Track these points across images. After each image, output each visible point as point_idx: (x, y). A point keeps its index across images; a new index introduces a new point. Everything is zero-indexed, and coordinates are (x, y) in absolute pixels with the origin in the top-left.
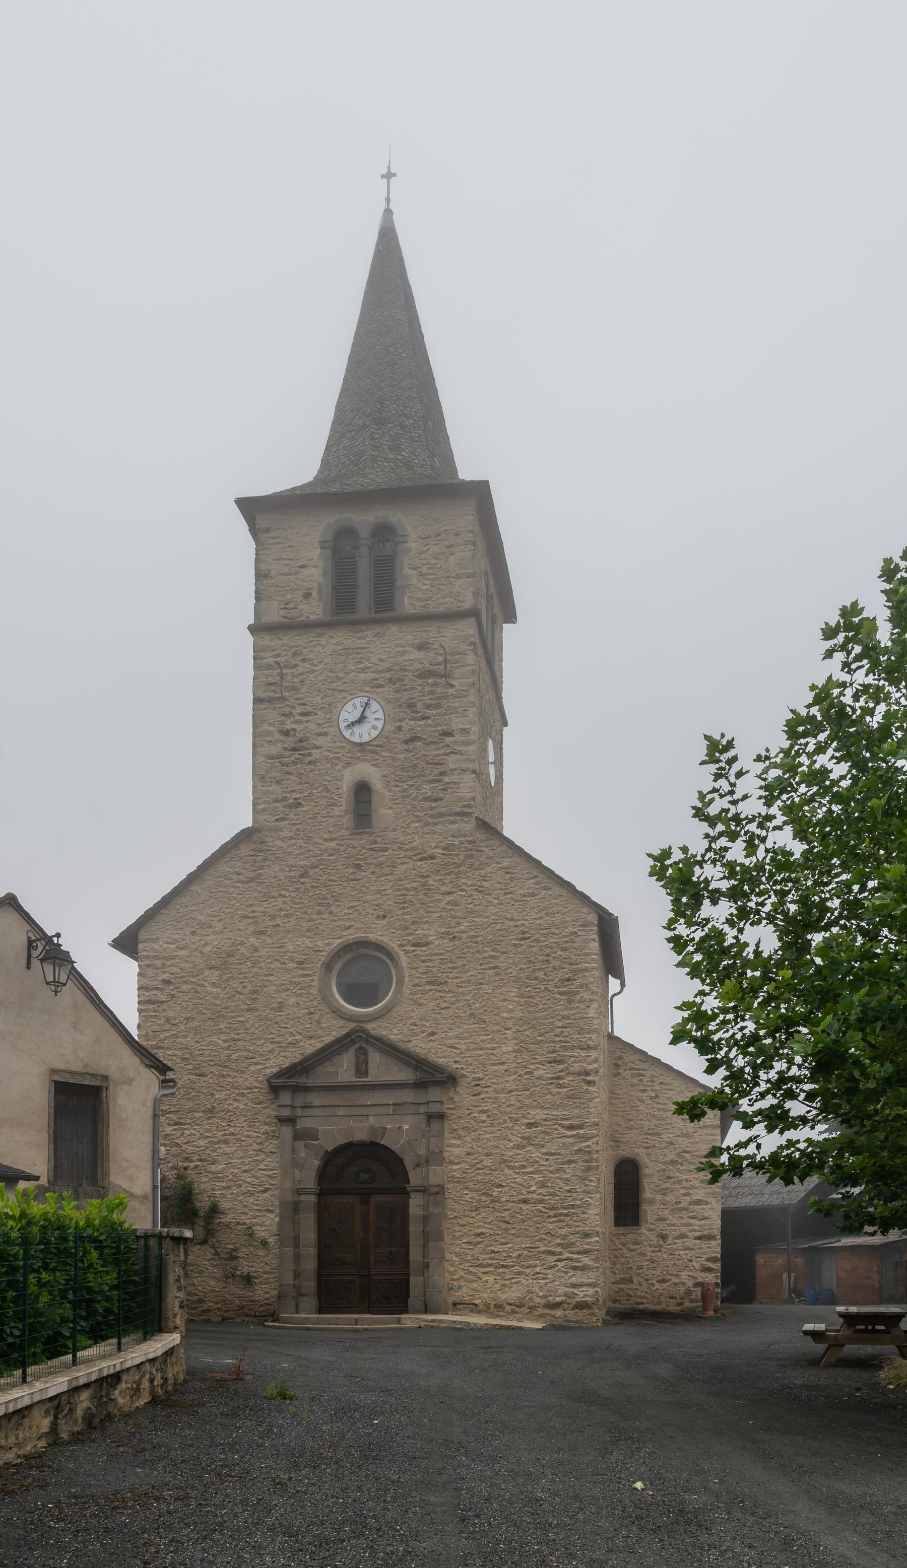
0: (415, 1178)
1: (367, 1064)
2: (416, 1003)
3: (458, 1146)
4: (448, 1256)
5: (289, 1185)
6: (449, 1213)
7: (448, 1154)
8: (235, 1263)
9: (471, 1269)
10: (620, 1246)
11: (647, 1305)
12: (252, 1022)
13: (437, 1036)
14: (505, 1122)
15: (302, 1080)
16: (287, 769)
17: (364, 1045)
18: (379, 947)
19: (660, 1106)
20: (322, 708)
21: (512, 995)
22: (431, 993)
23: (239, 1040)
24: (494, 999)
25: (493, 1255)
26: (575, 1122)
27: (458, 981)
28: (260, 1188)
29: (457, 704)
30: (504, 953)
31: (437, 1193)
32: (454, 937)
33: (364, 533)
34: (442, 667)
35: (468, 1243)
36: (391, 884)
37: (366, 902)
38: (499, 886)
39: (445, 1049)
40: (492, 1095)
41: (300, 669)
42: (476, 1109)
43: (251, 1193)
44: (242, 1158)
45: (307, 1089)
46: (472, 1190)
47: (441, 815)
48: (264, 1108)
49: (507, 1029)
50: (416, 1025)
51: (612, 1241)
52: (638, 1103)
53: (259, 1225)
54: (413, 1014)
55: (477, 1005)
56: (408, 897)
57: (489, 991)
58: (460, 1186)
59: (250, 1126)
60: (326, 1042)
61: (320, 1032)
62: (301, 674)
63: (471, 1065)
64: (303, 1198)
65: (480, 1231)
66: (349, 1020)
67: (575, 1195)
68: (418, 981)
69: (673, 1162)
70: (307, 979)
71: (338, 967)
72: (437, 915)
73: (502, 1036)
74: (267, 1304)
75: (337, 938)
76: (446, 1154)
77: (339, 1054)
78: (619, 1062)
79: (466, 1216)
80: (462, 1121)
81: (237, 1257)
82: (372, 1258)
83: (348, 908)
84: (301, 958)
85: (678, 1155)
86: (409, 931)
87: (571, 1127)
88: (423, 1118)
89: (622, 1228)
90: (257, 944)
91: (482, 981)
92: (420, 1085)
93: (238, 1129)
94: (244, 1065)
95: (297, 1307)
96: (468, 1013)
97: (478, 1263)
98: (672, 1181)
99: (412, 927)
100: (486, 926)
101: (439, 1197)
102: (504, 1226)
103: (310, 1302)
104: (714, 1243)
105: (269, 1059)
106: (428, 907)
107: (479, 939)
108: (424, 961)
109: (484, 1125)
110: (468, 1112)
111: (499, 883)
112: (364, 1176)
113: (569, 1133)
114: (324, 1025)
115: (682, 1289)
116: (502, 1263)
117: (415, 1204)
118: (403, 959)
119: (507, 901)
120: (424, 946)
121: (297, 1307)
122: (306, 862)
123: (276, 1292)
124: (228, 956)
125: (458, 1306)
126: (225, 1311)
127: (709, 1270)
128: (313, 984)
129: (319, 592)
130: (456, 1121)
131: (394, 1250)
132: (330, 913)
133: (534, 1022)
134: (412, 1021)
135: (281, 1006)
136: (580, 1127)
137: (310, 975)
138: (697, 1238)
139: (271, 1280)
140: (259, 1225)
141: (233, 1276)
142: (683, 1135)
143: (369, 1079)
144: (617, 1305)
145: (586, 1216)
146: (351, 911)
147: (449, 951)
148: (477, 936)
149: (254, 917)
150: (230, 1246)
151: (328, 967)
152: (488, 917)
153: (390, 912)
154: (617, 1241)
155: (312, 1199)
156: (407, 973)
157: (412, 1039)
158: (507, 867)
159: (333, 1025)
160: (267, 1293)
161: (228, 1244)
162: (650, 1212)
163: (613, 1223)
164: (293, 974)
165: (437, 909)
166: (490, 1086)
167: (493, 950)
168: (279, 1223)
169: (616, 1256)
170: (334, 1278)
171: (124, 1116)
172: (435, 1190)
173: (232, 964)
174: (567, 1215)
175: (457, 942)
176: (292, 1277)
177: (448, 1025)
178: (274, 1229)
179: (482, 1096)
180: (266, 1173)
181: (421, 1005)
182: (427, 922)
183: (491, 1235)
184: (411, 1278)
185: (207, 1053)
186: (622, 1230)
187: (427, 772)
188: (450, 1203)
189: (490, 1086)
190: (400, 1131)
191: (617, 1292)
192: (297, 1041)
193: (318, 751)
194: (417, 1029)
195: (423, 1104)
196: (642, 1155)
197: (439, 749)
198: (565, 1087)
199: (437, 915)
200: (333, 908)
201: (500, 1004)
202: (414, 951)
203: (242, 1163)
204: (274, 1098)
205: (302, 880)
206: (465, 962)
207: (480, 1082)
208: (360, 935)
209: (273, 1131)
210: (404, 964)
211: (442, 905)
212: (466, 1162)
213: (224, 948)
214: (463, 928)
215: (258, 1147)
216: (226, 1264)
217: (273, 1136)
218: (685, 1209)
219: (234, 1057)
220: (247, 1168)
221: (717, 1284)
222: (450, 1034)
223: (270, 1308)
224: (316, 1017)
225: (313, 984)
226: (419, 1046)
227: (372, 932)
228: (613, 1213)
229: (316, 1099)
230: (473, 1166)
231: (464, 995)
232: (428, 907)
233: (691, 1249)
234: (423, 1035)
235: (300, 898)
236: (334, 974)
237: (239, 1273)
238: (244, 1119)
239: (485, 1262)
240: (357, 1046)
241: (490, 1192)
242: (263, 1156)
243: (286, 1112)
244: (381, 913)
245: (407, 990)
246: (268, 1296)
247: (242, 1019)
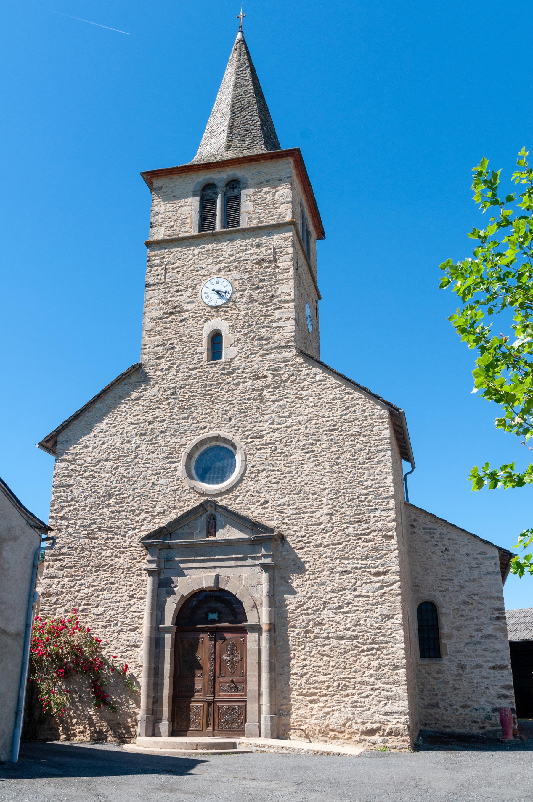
10: (427, 675)
11: (453, 729)
16: (166, 325)
18: (226, 440)
19: (450, 557)
20: (191, 287)
21: (326, 471)
23: (122, 511)
26: (381, 569)
29: (281, 278)
33: (221, 185)
34: (272, 256)
36: (235, 396)
39: (275, 513)
41: (177, 265)
47: (272, 349)
50: (252, 496)
51: (419, 670)
52: (432, 555)
60: (185, 511)
62: (178, 267)
67: (383, 631)
69: (465, 603)
78: (415, 524)
85: (469, 596)
87: (377, 574)
89: (427, 659)
91: (303, 462)
95: (154, 730)
98: (465, 618)
104: (505, 672)
108: (259, 449)
111: (314, 391)
113: (376, 579)
115: (483, 714)
122: (176, 385)
127: (505, 697)
129: (191, 219)
133: (345, 491)
134: (249, 492)
136: (385, 573)
138: (491, 668)
142: (470, 580)
144: (427, 728)
145: (394, 650)
147: (277, 441)
154: (423, 671)
158: (320, 381)
162: (448, 644)
163: (418, 655)
169: (423, 684)
171: (7, 566)
174: (378, 649)
182: (261, 422)
185: (98, 521)
186: (426, 661)
187: (262, 321)
191: (427, 716)
193: (187, 313)
196: (439, 598)
197: (269, 306)
198: (370, 541)
202: (251, 442)
205: (173, 397)
208: (213, 433)
211: (272, 409)
218: (479, 643)
219: (118, 524)
221: (512, 709)
226: (254, 513)
228: (418, 647)
230: (299, 607)
233: (487, 678)
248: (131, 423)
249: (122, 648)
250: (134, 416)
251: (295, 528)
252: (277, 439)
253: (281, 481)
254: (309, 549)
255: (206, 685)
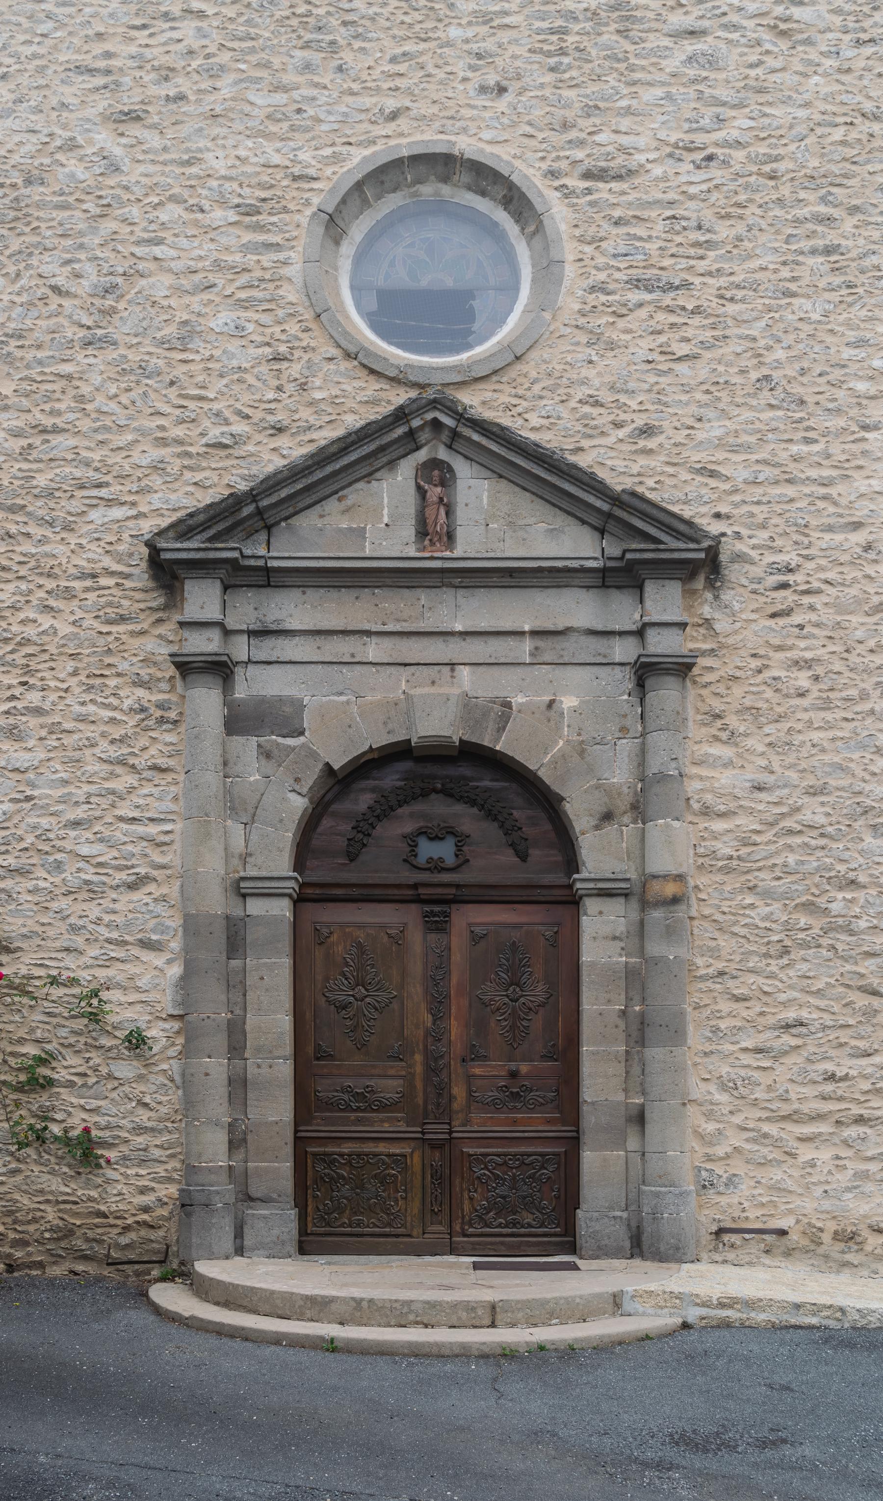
0: (600, 854)
1: (449, 512)
2: (595, 338)
3: (728, 764)
4: (698, 1090)
5: (214, 866)
6: (700, 961)
7: (697, 785)
8: (43, 1099)
9: (766, 1128)
12: (97, 380)
13: (661, 439)
14: (864, 696)
15: (256, 549)
17: (443, 454)
22: (643, 313)
23: (56, 430)
24: (829, 339)
25: (829, 1088)
27: (723, 281)
28: (123, 876)
30: (854, 210)
31: (675, 900)
32: (710, 158)
35: (759, 1051)
37: (449, 44)
38: (838, 20)
39: (685, 476)
40: (828, 616)
42: (780, 655)
43: (92, 891)
44: (65, 782)
45: (268, 578)
46: (768, 895)
48: (133, 634)
49: (865, 428)
50: (597, 404)
53: (119, 986)
54: (590, 372)
55: (780, 354)
56: (571, 39)
57: (815, 316)
58: (732, 882)
59: (90, 688)
61: (306, 414)
63: (763, 526)
64: (255, 907)
65: (791, 1015)
66: (395, 381)
68: (602, 276)
70: (267, 259)
71: (358, 231)
72: (659, 92)
73: (856, 448)
74: (145, 1224)
75: (359, 144)
76: (692, 787)
77: (368, 477)
79: (751, 971)
80: (738, 691)
81: (50, 1083)
82: (459, 1091)
83: (393, 60)
84: (251, 196)
86: (573, 134)
88: (625, 680)
90: (118, 151)
91: (793, 287)
92: (621, 577)
93: (53, 697)
94: (75, 506)
95: (239, 1234)
96: (754, 375)
97: (786, 1109)
99: (586, 124)
100: (801, 129)
101: (680, 912)
102: (862, 1001)
103: (280, 1220)
105: (149, 490)
106: (632, 69)
107: (782, 166)
109: (805, 702)
110: (755, 663)
112: (445, 850)
114: (318, 395)
116: (856, 1110)
117: (601, 934)
118: (559, 214)
119: (862, 64)
120: (619, 177)
121: (239, 1234)
123: (173, 1190)
124: (28, 182)
125: (726, 1238)
126: (16, 1243)
128: (286, 271)
130: (721, 690)
131: (524, 1068)
132: (340, 69)
135: (189, 332)
137: (276, 247)
139: (157, 1153)
140: (119, 986)
141: (40, 1138)
143: (458, 552)
146: (402, 68)
147: (692, 198)
148: (777, 159)
149: (108, 72)
150: (32, 1050)
151: (333, 225)
152: (807, 105)
153: (519, 77)
155: (282, 909)
156: (569, 251)
157: (585, 443)
159: (344, 394)
160: (143, 1191)
161: (21, 1041)
164: (224, 240)
165: (658, 77)
166: (819, 592)
167: (823, 200)
168: (185, 981)
170: (346, 1148)
172: (670, 889)
173: (39, 206)
175: (716, 173)
176: (225, 1147)
177: (693, 409)
178: (167, 1002)
179: (797, 618)
180: (140, 829)
181: (612, 346)
182: (628, 111)
183: (825, 1028)
184: (589, 1158)
188: (703, 932)
189: (819, 592)
190: (555, 708)
192: (237, 440)
194: (601, 416)
195: (621, 634)
199: (659, 92)
200: (347, 56)
201: (847, 353)
203: (62, 801)
204: (165, 607)
206: (740, 228)
207: (790, 578)
209: (160, 706)
210: (563, 227)
211: (672, 64)
212: (751, 812)
213: (16, 158)
214: (735, 134)
215: (114, 752)
216: (17, 1104)
217: (162, 720)
219: (41, 480)
220: (80, 813)
222: (700, 435)
223: (153, 1235)
224: (295, 369)
225: (286, 271)
226: (613, 463)
227: (465, 130)
229: (292, 609)
231: (740, 322)
232: (632, 69)
234: (621, 433)
235: (249, 22)
236: (348, 250)
237: (56, 1129)
238: (70, 665)
239: (805, 1108)
240: (422, 455)
241: (821, 901)
242: (131, 780)
243: (206, 644)
244: (492, 79)
245: (569, 302)
246: (147, 1199)
247: (67, 368)
248: (79, 69)
249: (94, 952)
250: (87, 39)
251: (763, 536)
252: (692, 190)
253: (707, 355)
254: (813, 617)
255: (419, 1085)
